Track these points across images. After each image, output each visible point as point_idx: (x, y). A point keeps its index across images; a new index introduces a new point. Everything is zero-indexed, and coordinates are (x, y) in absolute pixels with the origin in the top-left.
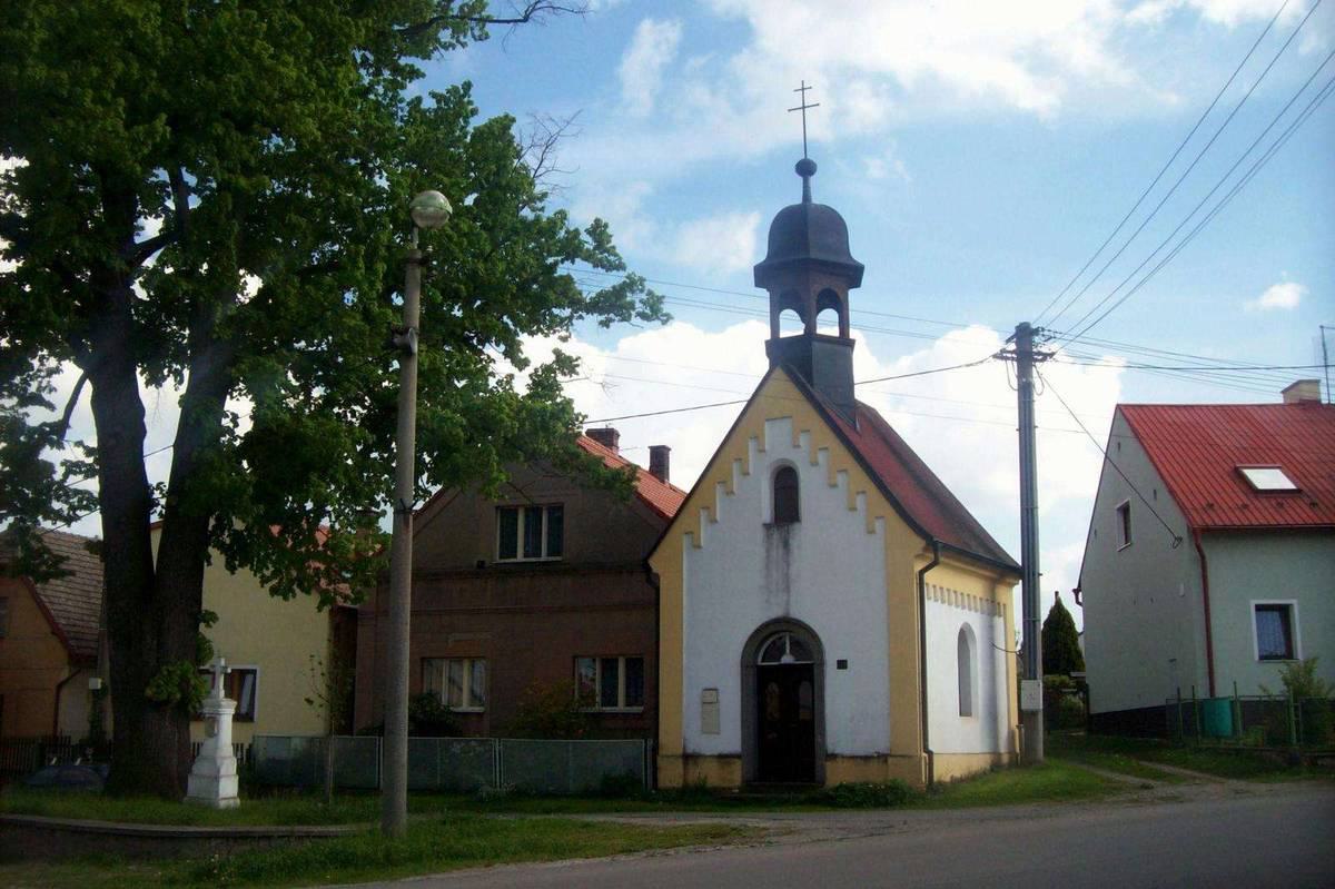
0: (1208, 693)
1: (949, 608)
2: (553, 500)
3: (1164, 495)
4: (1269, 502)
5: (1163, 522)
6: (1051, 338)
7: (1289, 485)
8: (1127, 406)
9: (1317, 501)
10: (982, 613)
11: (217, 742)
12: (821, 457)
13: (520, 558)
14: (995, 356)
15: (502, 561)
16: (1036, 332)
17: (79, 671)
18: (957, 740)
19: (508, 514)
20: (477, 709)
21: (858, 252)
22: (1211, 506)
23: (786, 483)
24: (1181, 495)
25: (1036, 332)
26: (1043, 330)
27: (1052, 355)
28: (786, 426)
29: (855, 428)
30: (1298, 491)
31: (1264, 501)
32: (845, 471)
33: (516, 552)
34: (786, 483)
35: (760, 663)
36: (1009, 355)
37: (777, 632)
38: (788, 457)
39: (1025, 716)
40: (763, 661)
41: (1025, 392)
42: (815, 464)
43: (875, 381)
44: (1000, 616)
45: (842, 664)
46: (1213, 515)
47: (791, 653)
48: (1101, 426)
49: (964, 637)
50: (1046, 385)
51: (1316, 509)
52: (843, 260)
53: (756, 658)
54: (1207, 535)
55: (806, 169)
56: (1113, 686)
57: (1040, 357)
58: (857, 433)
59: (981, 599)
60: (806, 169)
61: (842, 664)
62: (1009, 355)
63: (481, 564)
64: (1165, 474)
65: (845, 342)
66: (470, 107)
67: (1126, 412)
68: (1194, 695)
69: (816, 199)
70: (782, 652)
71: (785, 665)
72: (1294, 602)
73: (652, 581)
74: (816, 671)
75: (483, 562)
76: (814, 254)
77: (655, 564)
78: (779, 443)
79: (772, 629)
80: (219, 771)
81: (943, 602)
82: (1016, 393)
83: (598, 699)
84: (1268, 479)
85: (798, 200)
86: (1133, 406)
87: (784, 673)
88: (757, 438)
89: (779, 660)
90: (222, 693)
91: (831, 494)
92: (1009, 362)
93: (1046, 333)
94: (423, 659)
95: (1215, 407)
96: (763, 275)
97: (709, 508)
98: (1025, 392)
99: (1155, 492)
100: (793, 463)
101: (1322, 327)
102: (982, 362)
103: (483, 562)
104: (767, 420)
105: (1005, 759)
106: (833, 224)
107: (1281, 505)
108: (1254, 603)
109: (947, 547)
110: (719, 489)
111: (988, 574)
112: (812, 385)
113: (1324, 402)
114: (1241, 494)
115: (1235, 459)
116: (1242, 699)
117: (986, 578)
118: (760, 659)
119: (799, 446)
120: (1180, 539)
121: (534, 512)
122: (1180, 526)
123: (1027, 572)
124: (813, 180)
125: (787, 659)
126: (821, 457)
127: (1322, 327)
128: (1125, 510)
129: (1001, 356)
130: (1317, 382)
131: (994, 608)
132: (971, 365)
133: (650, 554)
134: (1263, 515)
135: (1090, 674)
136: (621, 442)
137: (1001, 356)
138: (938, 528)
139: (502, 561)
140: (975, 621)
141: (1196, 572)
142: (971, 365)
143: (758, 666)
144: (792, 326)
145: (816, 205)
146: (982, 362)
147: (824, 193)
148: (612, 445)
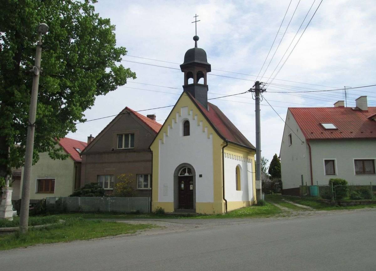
0: (311, 184)
1: (232, 160)
2: (132, 132)
3: (300, 130)
4: (329, 132)
5: (299, 138)
6: (265, 85)
7: (334, 127)
8: (291, 108)
9: (342, 131)
10: (242, 161)
11: (6, 201)
12: (196, 117)
13: (123, 148)
14: (249, 91)
15: (119, 149)
16: (260, 84)
17: (14, 181)
18: (234, 199)
19: (120, 136)
20: (112, 189)
21: (209, 61)
22: (312, 133)
23: (186, 125)
24: (304, 130)
25: (260, 84)
26: (262, 83)
27: (265, 90)
28: (186, 109)
29: (207, 108)
30: (337, 129)
31: (327, 131)
32: (202, 121)
33: (122, 146)
34: (186, 125)
35: (179, 175)
36: (253, 90)
37: (183, 167)
38: (186, 117)
39: (258, 191)
40: (180, 175)
41: (257, 100)
42: (194, 119)
43: (214, 97)
44: (250, 163)
45: (201, 176)
46: (312, 135)
47: (188, 172)
48: (93, 6)
49: (238, 169)
50: (263, 98)
51: (342, 134)
52: (206, 63)
53: (178, 174)
54: (310, 141)
55: (196, 39)
56: (289, 181)
57: (262, 91)
58: (208, 111)
59: (241, 157)
60: (196, 39)
61: (201, 176)
62: (253, 90)
63: (113, 150)
64: (300, 125)
65: (205, 86)
66: (78, 9)
67: (290, 109)
68: (306, 185)
69: (199, 47)
70: (185, 172)
72: (335, 159)
73: (151, 152)
74: (194, 177)
75: (113, 149)
76: (196, 61)
77: (152, 148)
79: (184, 165)
80: (5, 209)
81: (228, 158)
82: (255, 100)
83: (44, 189)
84: (328, 126)
85: (193, 47)
86: (293, 108)
87: (185, 178)
88: (179, 112)
89: (184, 175)
90: (8, 186)
91: (199, 127)
92: (253, 92)
93: (263, 84)
94: (137, 174)
95: (315, 108)
96: (183, 67)
97: (166, 132)
98: (257, 100)
99: (297, 130)
100: (187, 119)
101: (345, 87)
102: (245, 92)
103: (113, 149)
105: (256, 202)
106: (202, 54)
107: (332, 133)
108: (324, 159)
110: (169, 127)
111: (245, 150)
112: (194, 97)
113: (345, 106)
114: (321, 130)
115: (319, 121)
116: (319, 186)
117: (246, 152)
118: (179, 174)
119: (190, 114)
120: (304, 142)
121: (127, 136)
122: (304, 139)
123: (256, 150)
124: (198, 42)
125: (187, 174)
126: (196, 117)
127: (345, 87)
128: (290, 136)
129: (250, 90)
130: (344, 101)
131: (246, 160)
132: (243, 93)
134: (327, 135)
135: (283, 179)
136: (156, 118)
137: (250, 90)
138: (230, 137)
139: (119, 149)
140: (241, 163)
141: (308, 151)
142: (243, 93)
144: (191, 81)
145: (198, 48)
146: (245, 92)
147: (201, 45)
148: (153, 119)
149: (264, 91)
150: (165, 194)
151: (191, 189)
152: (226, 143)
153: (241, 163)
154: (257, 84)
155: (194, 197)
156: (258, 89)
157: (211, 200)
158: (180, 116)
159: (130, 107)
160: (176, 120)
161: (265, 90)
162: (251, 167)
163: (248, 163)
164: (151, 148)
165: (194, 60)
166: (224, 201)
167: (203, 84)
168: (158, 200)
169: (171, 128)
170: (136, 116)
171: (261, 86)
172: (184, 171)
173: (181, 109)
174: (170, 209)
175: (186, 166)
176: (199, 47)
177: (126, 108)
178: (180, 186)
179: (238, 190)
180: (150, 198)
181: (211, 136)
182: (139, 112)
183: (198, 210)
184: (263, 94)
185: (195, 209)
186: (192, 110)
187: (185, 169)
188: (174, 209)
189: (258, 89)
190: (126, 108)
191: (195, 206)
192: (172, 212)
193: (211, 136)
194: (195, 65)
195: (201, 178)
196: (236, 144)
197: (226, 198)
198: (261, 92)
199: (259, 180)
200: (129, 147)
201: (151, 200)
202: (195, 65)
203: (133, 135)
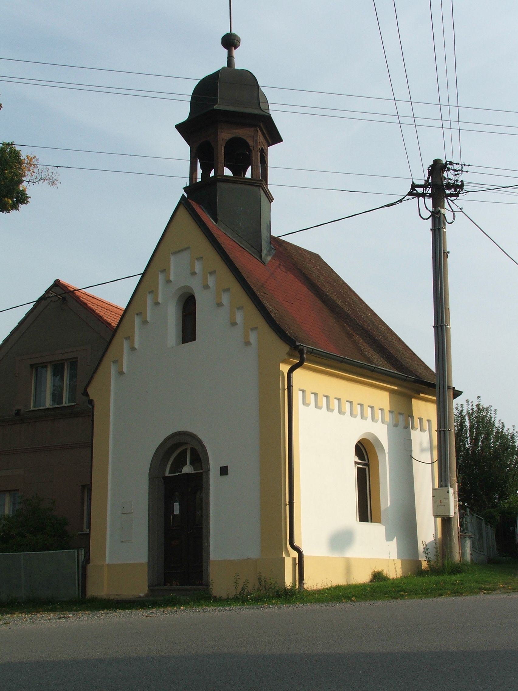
12: (211, 281)
14: (410, 194)
23: (188, 305)
26: (451, 163)
28: (186, 256)
34: (188, 305)
35: (167, 474)
41: (438, 222)
42: (206, 287)
47: (191, 464)
49: (364, 450)
52: (256, 112)
53: (165, 471)
55: (230, 42)
60: (230, 42)
63: (18, 413)
71: (187, 474)
75: (19, 411)
78: (181, 272)
87: (181, 479)
88: (165, 271)
89: (181, 472)
91: (223, 315)
98: (438, 222)
102: (401, 201)
104: (175, 253)
105: (424, 565)
106: (247, 82)
109: (311, 352)
110: (137, 321)
117: (391, 392)
124: (236, 53)
125: (187, 469)
126: (211, 281)
131: (403, 419)
132: (392, 204)
133: (87, 386)
140: (381, 431)
142: (392, 204)
143: (165, 478)
146: (401, 201)
149: (459, 188)
150: (122, 538)
151: (175, 513)
152: (301, 354)
153: (381, 431)
154: (437, 168)
155: (205, 544)
156: (439, 185)
157: (253, 552)
158: (169, 281)
159: (65, 280)
160: (157, 297)
161: (462, 186)
162: (423, 440)
163: (413, 432)
164: (90, 391)
165: (216, 102)
166: (295, 554)
167: (250, 177)
168: (105, 561)
169: (145, 322)
170: (84, 305)
171: (448, 175)
172: (180, 462)
173: (173, 259)
174: (140, 588)
175: (186, 443)
176: (239, 65)
177: (57, 284)
178: (169, 509)
179: (367, 521)
180: (82, 552)
181: (253, 337)
182: (87, 291)
183: (219, 582)
184: (461, 201)
185: (207, 585)
186: (200, 259)
187: (184, 452)
188: (149, 586)
189: (439, 185)
190: (57, 284)
191: (208, 576)
192: (142, 595)
193: (253, 337)
194: (228, 125)
195: (224, 478)
196: (342, 361)
197: (296, 543)
198: (451, 195)
199: (446, 486)
200: (65, 402)
201: (87, 560)
202: (228, 125)
203: (73, 364)
